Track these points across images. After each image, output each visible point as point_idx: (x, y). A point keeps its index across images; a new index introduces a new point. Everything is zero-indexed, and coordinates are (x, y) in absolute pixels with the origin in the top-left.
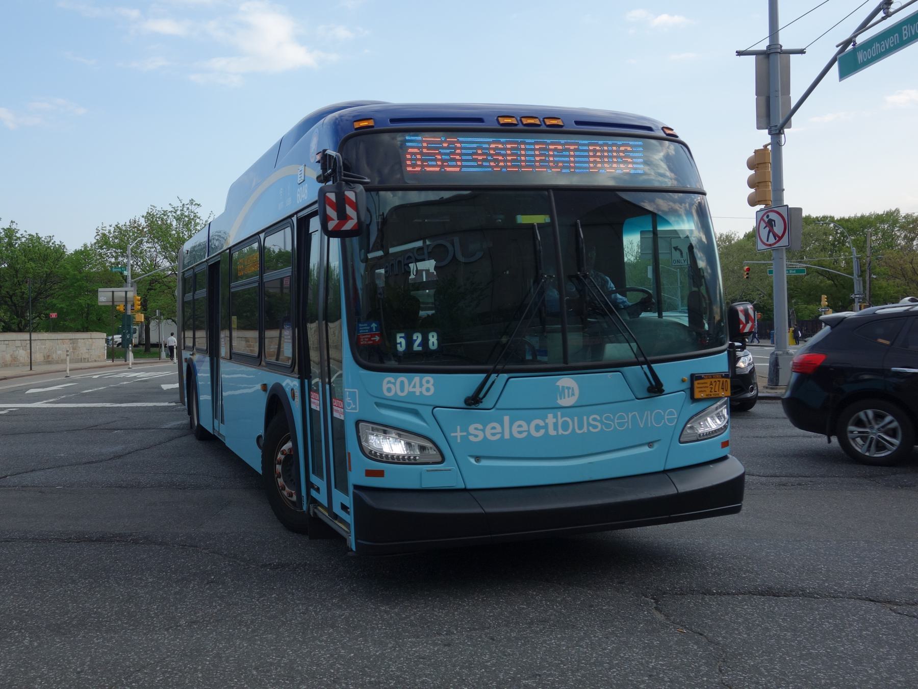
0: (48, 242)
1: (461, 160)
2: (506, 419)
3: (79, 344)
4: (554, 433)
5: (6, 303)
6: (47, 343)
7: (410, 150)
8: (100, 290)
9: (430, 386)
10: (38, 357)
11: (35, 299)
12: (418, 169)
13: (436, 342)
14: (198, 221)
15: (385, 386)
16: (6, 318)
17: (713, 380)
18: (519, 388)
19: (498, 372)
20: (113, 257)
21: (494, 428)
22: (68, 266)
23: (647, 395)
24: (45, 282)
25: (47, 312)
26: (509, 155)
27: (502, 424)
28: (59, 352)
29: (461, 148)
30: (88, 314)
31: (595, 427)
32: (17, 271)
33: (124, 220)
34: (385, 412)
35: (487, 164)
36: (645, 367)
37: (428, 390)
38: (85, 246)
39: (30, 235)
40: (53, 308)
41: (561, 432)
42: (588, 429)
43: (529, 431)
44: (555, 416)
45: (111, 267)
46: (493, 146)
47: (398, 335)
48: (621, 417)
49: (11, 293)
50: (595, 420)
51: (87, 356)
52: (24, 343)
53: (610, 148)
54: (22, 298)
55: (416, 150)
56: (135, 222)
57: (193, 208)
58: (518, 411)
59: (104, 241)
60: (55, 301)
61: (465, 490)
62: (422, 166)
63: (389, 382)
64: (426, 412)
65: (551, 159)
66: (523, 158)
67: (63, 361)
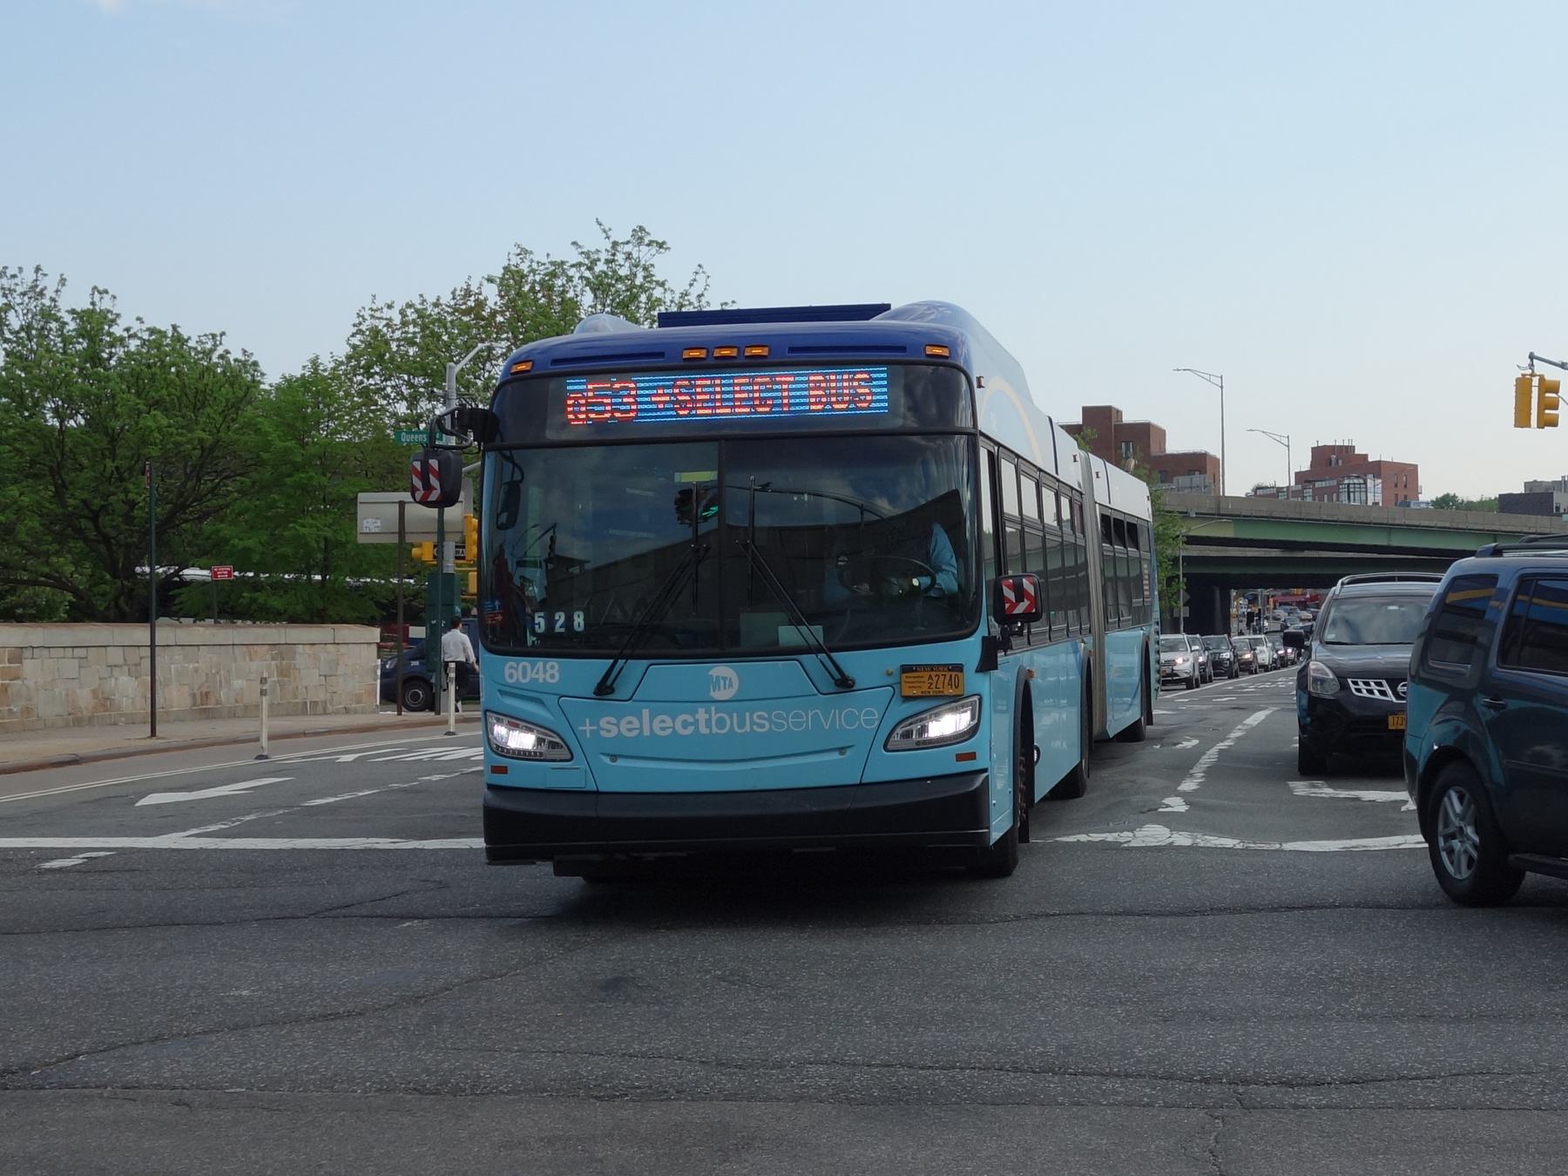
0: (208, 354)
2: (646, 713)
5: (79, 532)
6: (198, 653)
8: (362, 497)
10: (174, 697)
11: (167, 523)
14: (658, 293)
15: (507, 672)
16: (80, 580)
19: (628, 657)
20: (404, 398)
22: (266, 426)
23: (833, 688)
24: (198, 473)
27: (640, 719)
28: (238, 683)
31: (762, 726)
32: (113, 438)
33: (437, 284)
34: (509, 701)
36: (823, 656)
37: (552, 676)
38: (315, 363)
39: (152, 331)
41: (715, 730)
44: (708, 711)
45: (397, 429)
48: (797, 716)
49: (97, 503)
50: (760, 717)
51: (321, 696)
52: (133, 656)
54: (128, 519)
56: (468, 293)
57: (644, 254)
59: (373, 350)
60: (226, 530)
61: (598, 792)
64: (551, 700)
67: (251, 711)
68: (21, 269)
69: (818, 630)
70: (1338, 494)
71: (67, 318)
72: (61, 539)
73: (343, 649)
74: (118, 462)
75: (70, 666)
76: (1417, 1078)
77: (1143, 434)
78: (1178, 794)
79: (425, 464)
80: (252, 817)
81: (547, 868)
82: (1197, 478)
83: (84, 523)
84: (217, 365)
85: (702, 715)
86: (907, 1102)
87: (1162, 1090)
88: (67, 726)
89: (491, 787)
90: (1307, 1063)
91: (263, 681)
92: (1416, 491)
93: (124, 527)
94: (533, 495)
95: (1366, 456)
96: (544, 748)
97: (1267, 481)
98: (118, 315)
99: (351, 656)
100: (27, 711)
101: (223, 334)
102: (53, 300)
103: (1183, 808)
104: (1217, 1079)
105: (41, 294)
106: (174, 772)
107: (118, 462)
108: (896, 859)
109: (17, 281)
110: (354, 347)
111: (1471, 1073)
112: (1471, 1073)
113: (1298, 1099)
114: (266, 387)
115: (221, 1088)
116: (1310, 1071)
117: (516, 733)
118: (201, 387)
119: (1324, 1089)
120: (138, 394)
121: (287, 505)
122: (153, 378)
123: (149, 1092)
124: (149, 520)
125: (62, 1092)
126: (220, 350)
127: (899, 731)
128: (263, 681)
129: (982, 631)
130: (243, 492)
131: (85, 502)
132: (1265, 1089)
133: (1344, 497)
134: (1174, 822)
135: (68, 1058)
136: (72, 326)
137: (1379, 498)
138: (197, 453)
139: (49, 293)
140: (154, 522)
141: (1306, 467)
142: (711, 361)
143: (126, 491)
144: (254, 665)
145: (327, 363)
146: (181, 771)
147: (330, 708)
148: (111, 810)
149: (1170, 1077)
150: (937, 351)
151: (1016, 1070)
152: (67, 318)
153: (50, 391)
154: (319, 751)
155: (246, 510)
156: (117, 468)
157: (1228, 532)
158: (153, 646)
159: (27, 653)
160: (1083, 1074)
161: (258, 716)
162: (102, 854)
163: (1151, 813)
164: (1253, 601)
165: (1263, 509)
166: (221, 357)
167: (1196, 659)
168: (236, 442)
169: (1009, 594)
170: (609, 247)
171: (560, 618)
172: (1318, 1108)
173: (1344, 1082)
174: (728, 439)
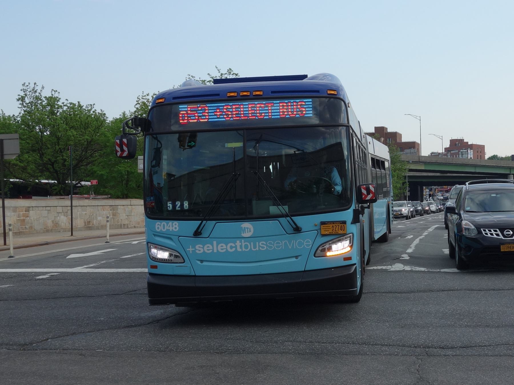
0: (89, 111)
1: (209, 116)
2: (215, 243)
5: (48, 170)
7: (181, 112)
9: (177, 226)
10: (79, 223)
11: (76, 166)
12: (186, 121)
13: (187, 206)
15: (157, 227)
17: (334, 225)
18: (223, 228)
19: (207, 220)
21: (208, 247)
22: (109, 135)
26: (234, 111)
28: (99, 218)
29: (208, 110)
30: (128, 181)
32: (58, 139)
35: (222, 116)
36: (288, 218)
37: (176, 228)
38: (124, 114)
39: (71, 103)
41: (244, 249)
42: (259, 249)
43: (226, 249)
44: (241, 242)
46: (225, 107)
47: (168, 203)
48: (278, 243)
49: (53, 160)
50: (262, 244)
51: (126, 222)
52: (65, 209)
55: (185, 112)
58: (221, 239)
60: (95, 168)
61: (195, 276)
62: (188, 120)
63: (158, 225)
64: (175, 238)
65: (258, 112)
66: (242, 113)
67: (104, 227)
68: (29, 83)
69: (286, 208)
70: (459, 155)
71: (44, 99)
72: (42, 171)
73: (133, 207)
74: (60, 146)
75: (45, 213)
76: (485, 346)
77: (394, 136)
78: (406, 253)
79: (121, 141)
80: (104, 262)
81: (174, 305)
82: (412, 150)
83: (49, 166)
84: (92, 114)
85: (238, 243)
86: (318, 354)
87: (401, 350)
89: (151, 274)
90: (448, 341)
91: (108, 217)
92: (484, 153)
93: (62, 167)
95: (467, 143)
96: (172, 258)
97: (435, 151)
98: (60, 99)
99: (134, 209)
100: (31, 227)
101: (94, 104)
102: (40, 93)
103: (408, 258)
104: (419, 347)
105: (36, 91)
107: (60, 146)
108: (318, 299)
109: (28, 87)
110: (137, 108)
111: (502, 344)
112: (502, 344)
113: (446, 353)
114: (108, 122)
117: (161, 252)
118: (87, 121)
119: (455, 349)
120: (67, 124)
121: (115, 160)
122: (71, 119)
124: (70, 166)
125: (43, 351)
126: (93, 110)
127: (320, 249)
128: (108, 217)
129: (353, 207)
130: (100, 156)
131: (49, 159)
133: (460, 156)
134: (405, 262)
135: (45, 340)
136: (46, 102)
137: (472, 156)
138: (86, 143)
139: (39, 91)
140: (72, 166)
141: (448, 146)
142: (239, 97)
143: (63, 156)
144: (105, 212)
145: (128, 114)
146: (81, 247)
147: (129, 226)
149: (404, 346)
151: (353, 343)
152: (44, 99)
153: (38, 124)
156: (60, 148)
157: (423, 168)
158: (72, 206)
159: (31, 209)
160: (375, 345)
161: (106, 229)
162: (56, 274)
163: (397, 259)
164: (431, 190)
165: (434, 160)
166: (93, 112)
167: (409, 209)
168: (98, 140)
169: (364, 192)
170: (220, 75)
171: (178, 204)
172: (453, 356)
173: (460, 347)
174: (248, 129)
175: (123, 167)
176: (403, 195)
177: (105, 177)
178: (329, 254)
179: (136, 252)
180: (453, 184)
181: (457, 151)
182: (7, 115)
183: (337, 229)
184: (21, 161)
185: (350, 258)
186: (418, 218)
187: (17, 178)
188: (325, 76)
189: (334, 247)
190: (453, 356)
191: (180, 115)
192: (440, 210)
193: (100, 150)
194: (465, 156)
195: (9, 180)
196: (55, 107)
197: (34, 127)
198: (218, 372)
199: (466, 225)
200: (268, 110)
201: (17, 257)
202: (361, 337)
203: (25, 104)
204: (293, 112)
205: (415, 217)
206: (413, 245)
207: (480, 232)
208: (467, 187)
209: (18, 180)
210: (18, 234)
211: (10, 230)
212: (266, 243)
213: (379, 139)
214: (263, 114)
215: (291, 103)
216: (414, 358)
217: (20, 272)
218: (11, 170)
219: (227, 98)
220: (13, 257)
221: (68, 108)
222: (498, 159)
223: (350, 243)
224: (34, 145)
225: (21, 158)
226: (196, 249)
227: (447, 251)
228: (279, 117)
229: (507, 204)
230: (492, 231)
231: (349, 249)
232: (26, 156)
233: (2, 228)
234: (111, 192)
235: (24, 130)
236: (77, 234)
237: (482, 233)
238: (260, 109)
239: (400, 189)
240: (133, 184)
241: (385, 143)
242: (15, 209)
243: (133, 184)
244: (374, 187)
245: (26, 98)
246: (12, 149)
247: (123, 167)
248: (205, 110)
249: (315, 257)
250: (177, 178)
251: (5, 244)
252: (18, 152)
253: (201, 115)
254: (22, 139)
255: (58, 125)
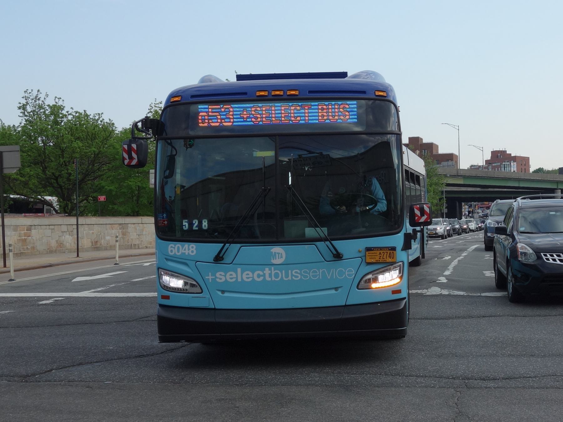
2: (239, 270)
3: (130, 230)
4: (270, 279)
9: (194, 249)
10: (85, 243)
11: (82, 181)
13: (207, 225)
15: (170, 249)
17: (382, 252)
19: (231, 243)
21: (231, 275)
23: (334, 259)
24: (93, 163)
25: (95, 195)
27: (236, 273)
28: (108, 238)
30: (138, 197)
31: (297, 277)
32: (63, 151)
36: (328, 243)
37: (192, 252)
39: (76, 112)
40: (100, 190)
41: (273, 278)
42: (292, 278)
43: (253, 277)
44: (270, 270)
46: (253, 109)
48: (315, 276)
49: (57, 174)
50: (295, 272)
51: (137, 242)
53: (333, 107)
54: (69, 180)
55: (205, 114)
58: (246, 265)
60: (103, 183)
61: (215, 309)
63: (172, 247)
64: (192, 264)
67: (112, 248)
68: (32, 90)
71: (47, 108)
72: (45, 187)
73: (145, 225)
74: (64, 159)
75: (48, 232)
76: (530, 377)
77: (430, 147)
78: (444, 276)
80: (113, 285)
82: (450, 163)
87: (439, 381)
88: (47, 253)
90: (490, 372)
92: (529, 166)
93: (67, 182)
94: (179, 162)
95: (510, 154)
96: (188, 287)
98: (64, 107)
99: (144, 228)
100: (33, 248)
101: (102, 113)
102: (43, 101)
103: (445, 281)
104: (458, 378)
105: (39, 99)
106: (85, 270)
107: (64, 159)
109: (31, 94)
115: (103, 382)
116: (491, 375)
118: (94, 132)
120: (72, 135)
121: (125, 174)
123: (77, 383)
124: (76, 180)
125: (47, 383)
126: (101, 119)
127: (364, 279)
128: (117, 237)
131: (53, 173)
132: (476, 382)
135: (49, 371)
136: (49, 110)
137: (515, 169)
138: (93, 156)
139: (42, 99)
141: (489, 158)
143: (67, 170)
144: (113, 231)
146: (88, 269)
148: (64, 283)
150: (381, 94)
151: (386, 375)
153: (40, 134)
154: (137, 262)
155: (111, 176)
156: (64, 161)
157: (461, 182)
158: (77, 225)
159: (33, 227)
160: (410, 376)
161: (115, 250)
162: (60, 299)
163: (434, 283)
164: (470, 206)
165: (474, 173)
166: (101, 121)
167: (445, 228)
169: (417, 212)
171: (196, 222)
172: (494, 388)
173: (503, 379)
175: (133, 183)
176: (440, 212)
177: (114, 193)
178: (374, 285)
179: (148, 275)
180: (492, 200)
181: (499, 164)
182: (6, 125)
183: (385, 257)
184: (22, 175)
185: (399, 291)
186: (455, 237)
187: (17, 195)
188: (368, 73)
189: (381, 277)
190: (494, 388)
191: (200, 117)
192: (480, 229)
193: (108, 163)
194: (507, 169)
195: (9, 196)
196: (58, 115)
197: (36, 139)
198: (237, 405)
199: (522, 248)
200: (305, 113)
201: (17, 280)
202: (394, 367)
203: (26, 114)
204: (335, 116)
205: (452, 236)
206: (451, 267)
207: (539, 258)
208: (519, 202)
209: (18, 196)
210: (18, 255)
211: (10, 251)
212: (301, 272)
213: (414, 151)
214: (298, 118)
215: (332, 105)
216: (452, 390)
217: (22, 297)
218: (11, 185)
219: (256, 98)
220: (13, 280)
221: (74, 117)
222: (544, 173)
223: (400, 273)
224: (37, 159)
225: (22, 172)
226: (217, 278)
227: (490, 274)
228: (317, 121)
229: (562, 224)
230: (555, 256)
231: (398, 280)
232: (28, 170)
233: (2, 248)
234: (121, 209)
235: (25, 141)
236: (83, 255)
237: (542, 258)
238: (295, 111)
239: (437, 205)
240: (144, 201)
241: (420, 156)
242: (16, 228)
243: (144, 201)
244: (429, 207)
245: (28, 107)
246: (12, 163)
247: (134, 181)
248: (230, 111)
249: (358, 288)
250: (187, 189)
251: (5, 266)
252: (19, 165)
253: (225, 117)
254: (23, 152)
255: (63, 136)
